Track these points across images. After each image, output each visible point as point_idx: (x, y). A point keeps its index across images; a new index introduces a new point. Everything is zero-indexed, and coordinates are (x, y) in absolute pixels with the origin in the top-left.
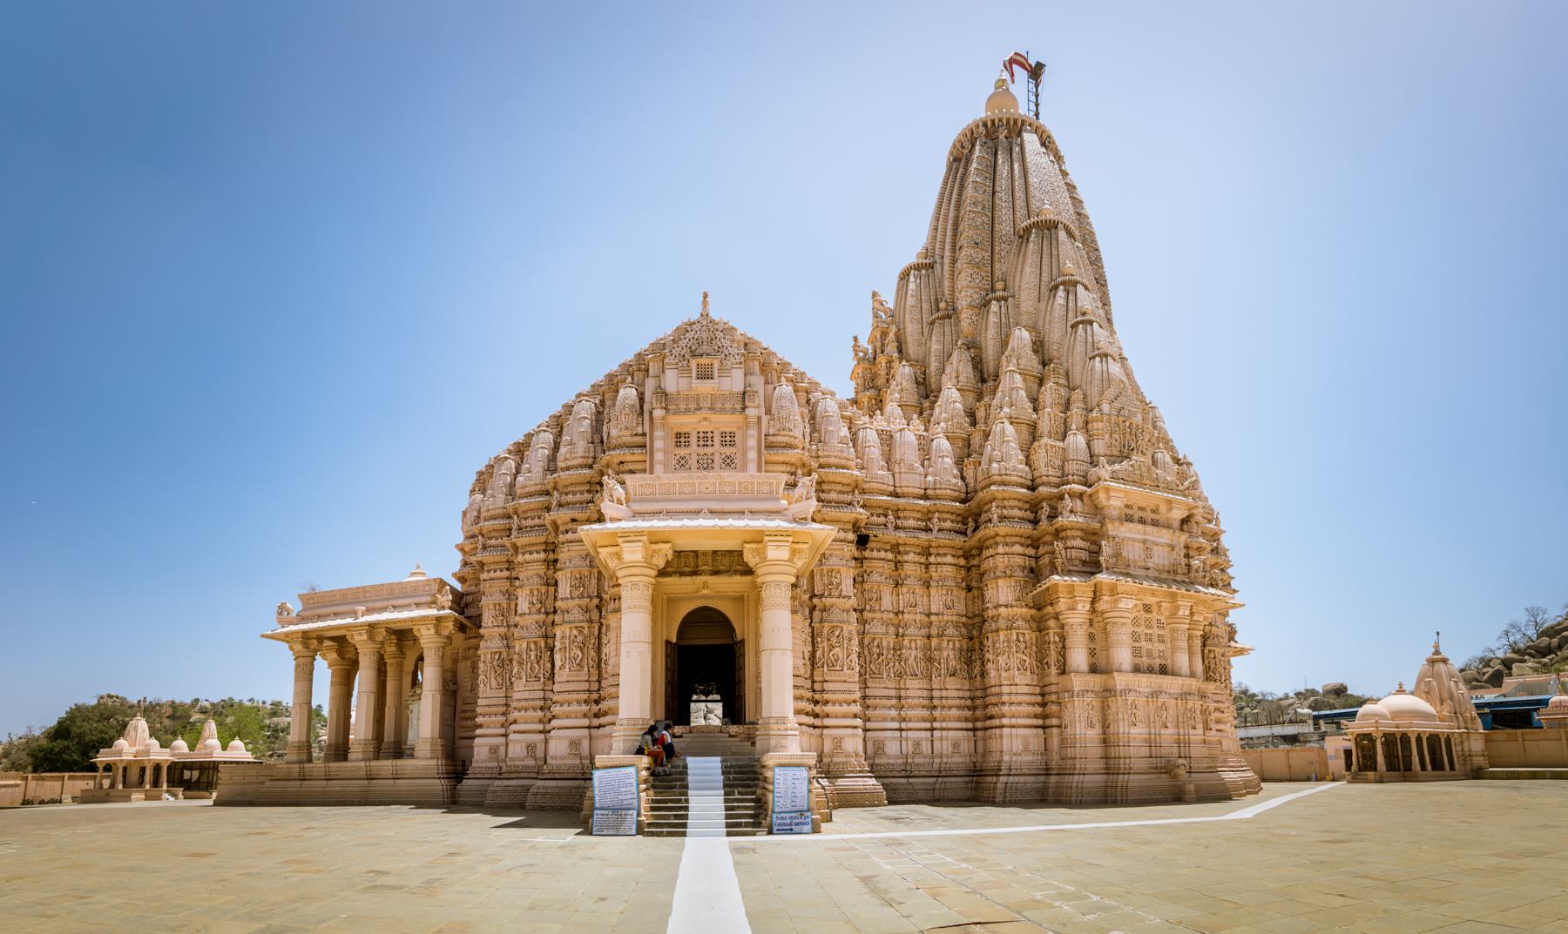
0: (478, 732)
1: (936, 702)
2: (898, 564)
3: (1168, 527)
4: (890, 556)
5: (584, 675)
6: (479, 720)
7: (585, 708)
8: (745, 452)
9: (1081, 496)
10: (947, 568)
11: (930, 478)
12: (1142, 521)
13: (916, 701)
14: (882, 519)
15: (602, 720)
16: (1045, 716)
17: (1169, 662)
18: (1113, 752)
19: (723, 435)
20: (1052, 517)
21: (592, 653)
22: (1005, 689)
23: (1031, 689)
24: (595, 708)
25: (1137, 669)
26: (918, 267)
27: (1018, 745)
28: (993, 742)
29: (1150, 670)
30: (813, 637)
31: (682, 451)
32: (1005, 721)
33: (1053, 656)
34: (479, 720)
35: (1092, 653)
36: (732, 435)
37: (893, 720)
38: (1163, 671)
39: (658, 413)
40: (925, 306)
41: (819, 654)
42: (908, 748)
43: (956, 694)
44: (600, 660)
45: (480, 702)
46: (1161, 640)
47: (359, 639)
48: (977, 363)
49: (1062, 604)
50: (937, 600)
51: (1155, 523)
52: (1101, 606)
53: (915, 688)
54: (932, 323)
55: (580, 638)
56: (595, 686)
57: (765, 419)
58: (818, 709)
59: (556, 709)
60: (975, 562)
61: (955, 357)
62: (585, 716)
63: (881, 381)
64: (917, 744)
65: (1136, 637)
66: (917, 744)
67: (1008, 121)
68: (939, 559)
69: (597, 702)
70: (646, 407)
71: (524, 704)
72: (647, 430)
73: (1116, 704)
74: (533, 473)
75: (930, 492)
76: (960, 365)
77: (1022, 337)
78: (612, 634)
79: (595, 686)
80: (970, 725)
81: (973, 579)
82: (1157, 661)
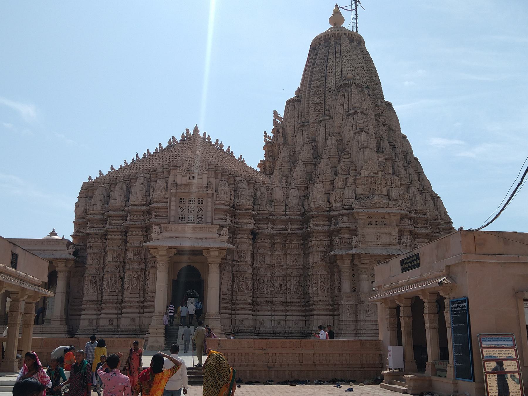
0: (83, 312)
6: (84, 307)
7: (137, 305)
14: (266, 226)
15: (145, 310)
16: (334, 310)
20: (336, 224)
22: (315, 299)
31: (182, 205)
32: (315, 313)
39: (173, 191)
42: (275, 323)
44: (145, 285)
45: (84, 299)
48: (315, 149)
50: (290, 261)
52: (356, 262)
54: (298, 128)
55: (136, 276)
56: (142, 296)
59: (124, 304)
61: (304, 148)
62: (137, 308)
64: (279, 322)
66: (279, 322)
69: (143, 303)
70: (169, 188)
77: (332, 141)
79: (142, 296)
80: (303, 314)
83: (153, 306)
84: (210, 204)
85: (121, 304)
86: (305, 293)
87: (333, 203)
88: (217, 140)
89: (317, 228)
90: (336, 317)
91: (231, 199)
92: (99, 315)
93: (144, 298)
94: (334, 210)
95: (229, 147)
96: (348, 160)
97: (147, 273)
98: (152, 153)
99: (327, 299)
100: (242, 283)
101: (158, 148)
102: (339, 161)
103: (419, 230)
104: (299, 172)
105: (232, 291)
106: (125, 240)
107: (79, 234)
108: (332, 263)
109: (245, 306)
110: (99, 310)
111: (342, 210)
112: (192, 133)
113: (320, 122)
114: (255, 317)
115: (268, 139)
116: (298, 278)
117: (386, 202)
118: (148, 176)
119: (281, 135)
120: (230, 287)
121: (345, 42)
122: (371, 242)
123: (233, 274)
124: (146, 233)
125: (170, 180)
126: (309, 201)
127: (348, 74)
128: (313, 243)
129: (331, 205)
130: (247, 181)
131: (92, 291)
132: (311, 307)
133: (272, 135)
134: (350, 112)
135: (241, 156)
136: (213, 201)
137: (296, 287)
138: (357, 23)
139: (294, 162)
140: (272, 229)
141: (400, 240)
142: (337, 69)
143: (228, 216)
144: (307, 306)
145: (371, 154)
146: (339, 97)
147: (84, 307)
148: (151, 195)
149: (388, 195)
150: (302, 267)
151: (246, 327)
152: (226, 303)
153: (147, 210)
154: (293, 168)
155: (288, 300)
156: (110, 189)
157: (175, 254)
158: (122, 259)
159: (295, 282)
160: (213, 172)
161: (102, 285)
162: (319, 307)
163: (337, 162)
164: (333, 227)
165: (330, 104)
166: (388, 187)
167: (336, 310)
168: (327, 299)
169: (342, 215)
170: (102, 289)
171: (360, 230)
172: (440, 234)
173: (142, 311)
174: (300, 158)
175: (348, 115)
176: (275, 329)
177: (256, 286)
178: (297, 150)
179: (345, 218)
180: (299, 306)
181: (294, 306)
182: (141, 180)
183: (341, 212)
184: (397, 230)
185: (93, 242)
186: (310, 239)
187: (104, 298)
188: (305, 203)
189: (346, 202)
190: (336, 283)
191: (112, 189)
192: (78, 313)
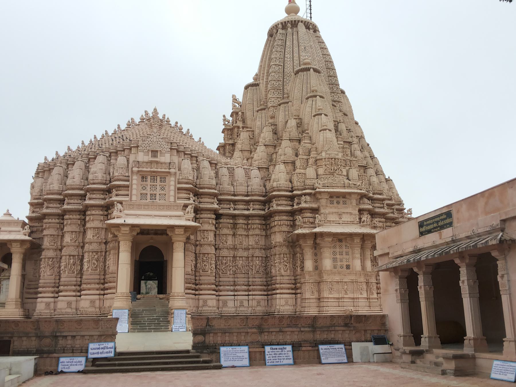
0: (40, 295)
4: (231, 221)
6: (40, 289)
8: (170, 186)
9: (309, 194)
14: (228, 206)
15: (106, 292)
16: (296, 289)
17: (351, 264)
18: (322, 304)
20: (299, 204)
21: (102, 264)
27: (283, 302)
28: (274, 301)
30: (196, 258)
32: (278, 291)
37: (231, 291)
40: (255, 103)
41: (198, 265)
44: (105, 266)
45: (40, 281)
50: (252, 241)
52: (318, 241)
55: (96, 257)
57: (178, 172)
59: (84, 286)
61: (264, 130)
64: (242, 302)
66: (242, 302)
72: (130, 175)
74: (76, 175)
75: (249, 193)
77: (292, 123)
80: (266, 293)
83: (115, 288)
84: (172, 183)
85: (80, 286)
86: (267, 273)
87: (295, 183)
88: (177, 123)
89: (280, 208)
90: (299, 295)
91: (194, 178)
92: (57, 298)
93: (104, 279)
94: (295, 190)
95: (188, 130)
96: (309, 141)
97: (108, 253)
98: (110, 134)
99: (290, 278)
100: (205, 263)
101: (117, 129)
102: (300, 143)
103: (377, 210)
104: (260, 154)
105: (195, 271)
106: (84, 219)
107: (34, 215)
108: (295, 243)
109: (209, 286)
110: (57, 293)
111: (304, 190)
112: (151, 115)
113: (280, 105)
114: (218, 297)
115: (227, 123)
116: (260, 259)
117: (347, 181)
118: (108, 155)
119: (240, 118)
120: (193, 267)
121: (301, 28)
122: (333, 221)
123: (196, 254)
124: (106, 213)
125: (132, 158)
126: (271, 181)
127: (305, 59)
128: (276, 223)
129: (293, 185)
130: (209, 162)
131: (49, 274)
132: (274, 286)
133: (231, 119)
134: (309, 95)
135: (200, 138)
136: (176, 180)
137: (258, 267)
138: (311, 13)
139: (254, 143)
140: (235, 209)
141: (360, 219)
142: (294, 55)
143: (191, 195)
144: (269, 285)
145: (331, 135)
146: (298, 81)
147: (40, 289)
148: (111, 174)
149: (347, 175)
150: (264, 247)
151: (210, 307)
152: (190, 283)
153: (107, 189)
154: (254, 150)
155: (250, 280)
156: (68, 168)
157: (138, 234)
158: (80, 240)
159: (257, 262)
160: (175, 151)
161: (60, 267)
162: (282, 285)
163: (298, 144)
164: (295, 207)
165: (288, 88)
166: (347, 168)
167: (297, 289)
168: (290, 278)
169: (305, 194)
170: (60, 272)
171: (322, 211)
172: (394, 214)
173: (102, 292)
174: (261, 140)
175: (307, 99)
176: (238, 309)
177: (218, 267)
178: (256, 133)
179: (308, 198)
180: (261, 285)
181: (257, 285)
182: (101, 158)
183: (304, 191)
184: (357, 209)
185: (50, 223)
186: (272, 219)
187: (61, 280)
188: (267, 183)
189: (308, 182)
190: (299, 262)
191: (70, 169)
192: (35, 296)
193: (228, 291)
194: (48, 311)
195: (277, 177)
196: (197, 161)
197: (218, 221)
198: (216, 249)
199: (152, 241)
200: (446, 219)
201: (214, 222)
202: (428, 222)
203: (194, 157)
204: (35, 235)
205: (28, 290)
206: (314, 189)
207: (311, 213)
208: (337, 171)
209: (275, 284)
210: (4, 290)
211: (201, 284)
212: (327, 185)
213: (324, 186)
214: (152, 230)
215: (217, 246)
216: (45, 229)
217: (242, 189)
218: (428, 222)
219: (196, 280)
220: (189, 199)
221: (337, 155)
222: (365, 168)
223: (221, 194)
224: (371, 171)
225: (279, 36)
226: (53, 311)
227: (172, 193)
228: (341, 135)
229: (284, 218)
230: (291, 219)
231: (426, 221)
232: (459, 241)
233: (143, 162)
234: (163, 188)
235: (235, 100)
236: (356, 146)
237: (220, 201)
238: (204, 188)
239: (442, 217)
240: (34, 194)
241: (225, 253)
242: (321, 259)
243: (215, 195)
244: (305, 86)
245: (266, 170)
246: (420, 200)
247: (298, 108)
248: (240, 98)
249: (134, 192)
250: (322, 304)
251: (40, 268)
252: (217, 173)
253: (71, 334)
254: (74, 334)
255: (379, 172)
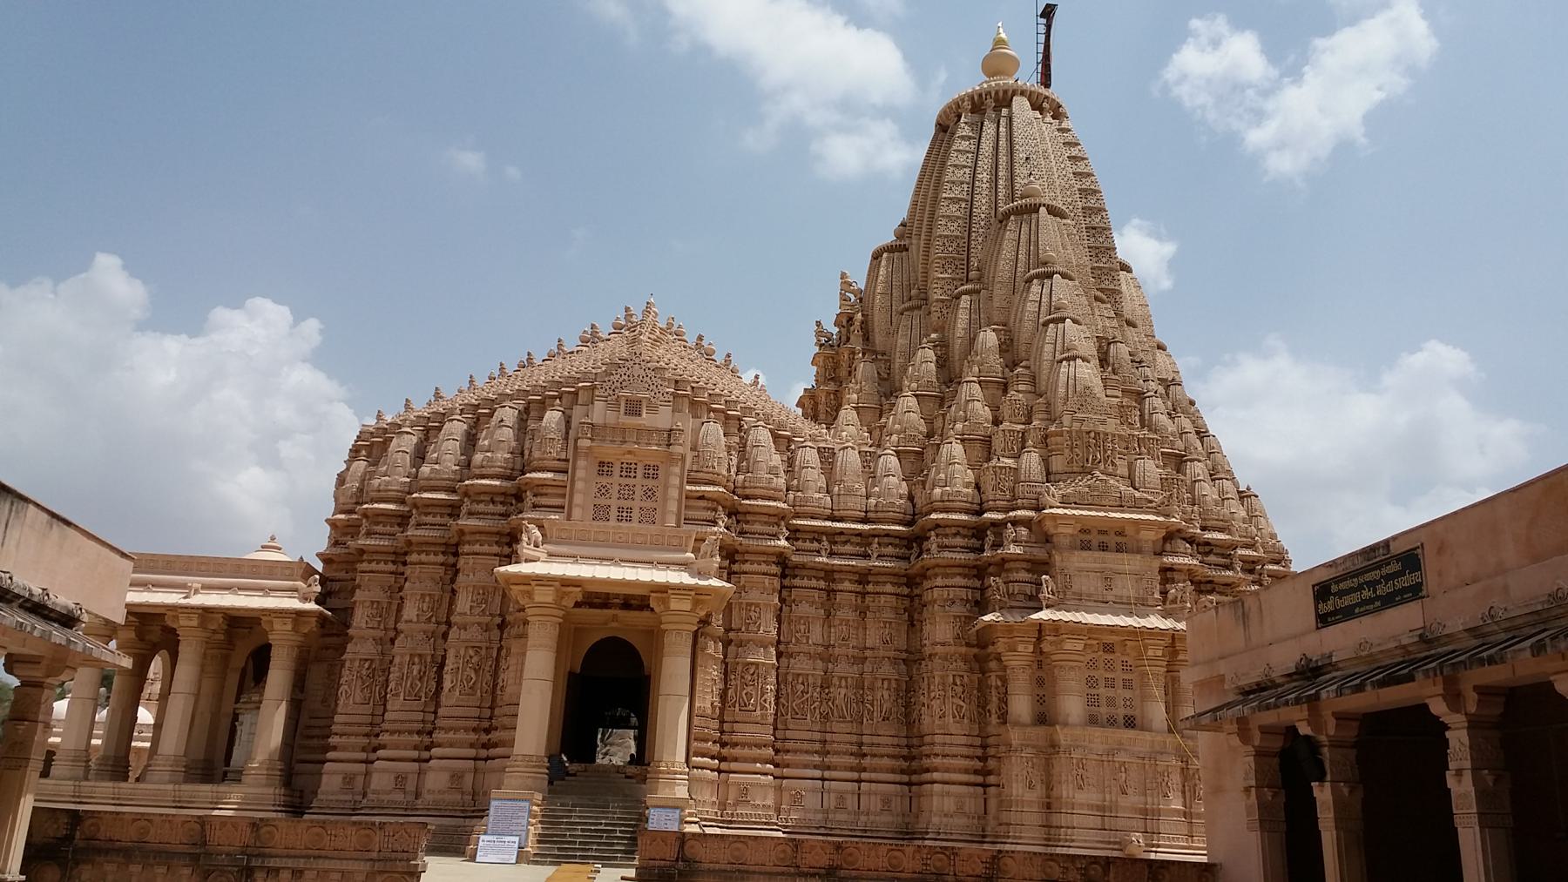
0: (330, 755)
1: (865, 749)
2: (830, 592)
3: (1139, 551)
4: (822, 584)
5: (475, 700)
6: (334, 740)
7: (472, 736)
8: (666, 487)
9: (1027, 523)
10: (886, 599)
11: (872, 501)
12: (1103, 547)
13: (843, 747)
14: (816, 544)
15: (492, 752)
16: (986, 772)
17: (1137, 713)
18: (1056, 819)
19: (647, 467)
20: (997, 545)
23: (970, 741)
24: (484, 738)
25: (1093, 721)
26: (890, 249)
27: (949, 804)
29: (1111, 722)
30: (726, 674)
31: (604, 480)
32: (936, 776)
33: (993, 706)
34: (334, 740)
35: (1040, 700)
36: (656, 468)
37: (815, 767)
38: (1130, 723)
43: (889, 740)
44: (495, 686)
45: (337, 718)
46: (1127, 685)
47: (184, 624)
49: (1000, 646)
51: (1119, 549)
53: (842, 734)
58: (725, 751)
59: (439, 736)
60: (917, 591)
63: (843, 373)
64: (841, 797)
65: (1091, 682)
67: (997, 93)
68: (879, 589)
71: (397, 726)
72: (570, 457)
73: (1061, 765)
75: (871, 515)
76: (926, 360)
77: (989, 338)
78: (512, 661)
79: (487, 713)
80: (905, 778)
81: (913, 613)
82: (1121, 712)
87: (989, 494)
88: (700, 338)
90: (992, 790)
91: (729, 471)
92: (427, 761)
94: (990, 510)
99: (970, 741)
102: (1005, 391)
105: (722, 710)
117: (1124, 488)
120: (717, 699)
131: (358, 700)
141: (1164, 593)
144: (914, 758)
145: (1088, 373)
155: (866, 739)
167: (990, 773)
169: (1016, 522)
192: (320, 757)
193: (806, 766)
194: (348, 797)
195: (942, 476)
196: (740, 429)
197: (786, 582)
198: (779, 655)
199: (614, 625)
200: (1400, 574)
201: (776, 583)
202: (1342, 586)
203: (734, 423)
204: (334, 602)
205: (306, 742)
206: (1038, 509)
207: (1028, 571)
208: (1102, 466)
209: (928, 756)
210: (244, 738)
211: (735, 745)
212: (1072, 499)
213: (1065, 502)
214: (617, 596)
215: (782, 647)
216: (359, 587)
217: (855, 505)
218: (1342, 586)
219: (722, 732)
220: (715, 523)
221: (1103, 422)
222: (1179, 461)
223: (797, 516)
224: (1198, 469)
225: (964, 130)
226: (359, 798)
227: (673, 506)
228: (1114, 372)
229: (959, 580)
230: (978, 584)
231: (1337, 583)
232: (1446, 644)
233: (605, 426)
234: (649, 494)
235: (846, 284)
236: (1158, 402)
237: (795, 534)
238: (755, 497)
239: (1386, 570)
240: (342, 500)
241: (801, 665)
242: (1054, 695)
243: (781, 517)
244: (1023, 251)
245: (917, 462)
246: (1321, 531)
247: (1004, 304)
248: (860, 280)
249: (578, 499)
250: (1056, 819)
251: (339, 685)
252: (790, 462)
253: (290, 863)
254: (301, 864)
255: (1217, 473)
